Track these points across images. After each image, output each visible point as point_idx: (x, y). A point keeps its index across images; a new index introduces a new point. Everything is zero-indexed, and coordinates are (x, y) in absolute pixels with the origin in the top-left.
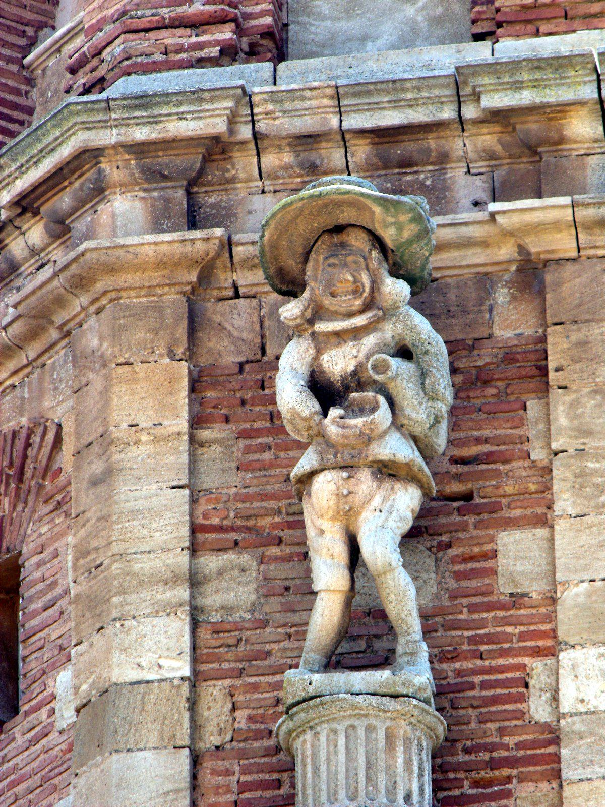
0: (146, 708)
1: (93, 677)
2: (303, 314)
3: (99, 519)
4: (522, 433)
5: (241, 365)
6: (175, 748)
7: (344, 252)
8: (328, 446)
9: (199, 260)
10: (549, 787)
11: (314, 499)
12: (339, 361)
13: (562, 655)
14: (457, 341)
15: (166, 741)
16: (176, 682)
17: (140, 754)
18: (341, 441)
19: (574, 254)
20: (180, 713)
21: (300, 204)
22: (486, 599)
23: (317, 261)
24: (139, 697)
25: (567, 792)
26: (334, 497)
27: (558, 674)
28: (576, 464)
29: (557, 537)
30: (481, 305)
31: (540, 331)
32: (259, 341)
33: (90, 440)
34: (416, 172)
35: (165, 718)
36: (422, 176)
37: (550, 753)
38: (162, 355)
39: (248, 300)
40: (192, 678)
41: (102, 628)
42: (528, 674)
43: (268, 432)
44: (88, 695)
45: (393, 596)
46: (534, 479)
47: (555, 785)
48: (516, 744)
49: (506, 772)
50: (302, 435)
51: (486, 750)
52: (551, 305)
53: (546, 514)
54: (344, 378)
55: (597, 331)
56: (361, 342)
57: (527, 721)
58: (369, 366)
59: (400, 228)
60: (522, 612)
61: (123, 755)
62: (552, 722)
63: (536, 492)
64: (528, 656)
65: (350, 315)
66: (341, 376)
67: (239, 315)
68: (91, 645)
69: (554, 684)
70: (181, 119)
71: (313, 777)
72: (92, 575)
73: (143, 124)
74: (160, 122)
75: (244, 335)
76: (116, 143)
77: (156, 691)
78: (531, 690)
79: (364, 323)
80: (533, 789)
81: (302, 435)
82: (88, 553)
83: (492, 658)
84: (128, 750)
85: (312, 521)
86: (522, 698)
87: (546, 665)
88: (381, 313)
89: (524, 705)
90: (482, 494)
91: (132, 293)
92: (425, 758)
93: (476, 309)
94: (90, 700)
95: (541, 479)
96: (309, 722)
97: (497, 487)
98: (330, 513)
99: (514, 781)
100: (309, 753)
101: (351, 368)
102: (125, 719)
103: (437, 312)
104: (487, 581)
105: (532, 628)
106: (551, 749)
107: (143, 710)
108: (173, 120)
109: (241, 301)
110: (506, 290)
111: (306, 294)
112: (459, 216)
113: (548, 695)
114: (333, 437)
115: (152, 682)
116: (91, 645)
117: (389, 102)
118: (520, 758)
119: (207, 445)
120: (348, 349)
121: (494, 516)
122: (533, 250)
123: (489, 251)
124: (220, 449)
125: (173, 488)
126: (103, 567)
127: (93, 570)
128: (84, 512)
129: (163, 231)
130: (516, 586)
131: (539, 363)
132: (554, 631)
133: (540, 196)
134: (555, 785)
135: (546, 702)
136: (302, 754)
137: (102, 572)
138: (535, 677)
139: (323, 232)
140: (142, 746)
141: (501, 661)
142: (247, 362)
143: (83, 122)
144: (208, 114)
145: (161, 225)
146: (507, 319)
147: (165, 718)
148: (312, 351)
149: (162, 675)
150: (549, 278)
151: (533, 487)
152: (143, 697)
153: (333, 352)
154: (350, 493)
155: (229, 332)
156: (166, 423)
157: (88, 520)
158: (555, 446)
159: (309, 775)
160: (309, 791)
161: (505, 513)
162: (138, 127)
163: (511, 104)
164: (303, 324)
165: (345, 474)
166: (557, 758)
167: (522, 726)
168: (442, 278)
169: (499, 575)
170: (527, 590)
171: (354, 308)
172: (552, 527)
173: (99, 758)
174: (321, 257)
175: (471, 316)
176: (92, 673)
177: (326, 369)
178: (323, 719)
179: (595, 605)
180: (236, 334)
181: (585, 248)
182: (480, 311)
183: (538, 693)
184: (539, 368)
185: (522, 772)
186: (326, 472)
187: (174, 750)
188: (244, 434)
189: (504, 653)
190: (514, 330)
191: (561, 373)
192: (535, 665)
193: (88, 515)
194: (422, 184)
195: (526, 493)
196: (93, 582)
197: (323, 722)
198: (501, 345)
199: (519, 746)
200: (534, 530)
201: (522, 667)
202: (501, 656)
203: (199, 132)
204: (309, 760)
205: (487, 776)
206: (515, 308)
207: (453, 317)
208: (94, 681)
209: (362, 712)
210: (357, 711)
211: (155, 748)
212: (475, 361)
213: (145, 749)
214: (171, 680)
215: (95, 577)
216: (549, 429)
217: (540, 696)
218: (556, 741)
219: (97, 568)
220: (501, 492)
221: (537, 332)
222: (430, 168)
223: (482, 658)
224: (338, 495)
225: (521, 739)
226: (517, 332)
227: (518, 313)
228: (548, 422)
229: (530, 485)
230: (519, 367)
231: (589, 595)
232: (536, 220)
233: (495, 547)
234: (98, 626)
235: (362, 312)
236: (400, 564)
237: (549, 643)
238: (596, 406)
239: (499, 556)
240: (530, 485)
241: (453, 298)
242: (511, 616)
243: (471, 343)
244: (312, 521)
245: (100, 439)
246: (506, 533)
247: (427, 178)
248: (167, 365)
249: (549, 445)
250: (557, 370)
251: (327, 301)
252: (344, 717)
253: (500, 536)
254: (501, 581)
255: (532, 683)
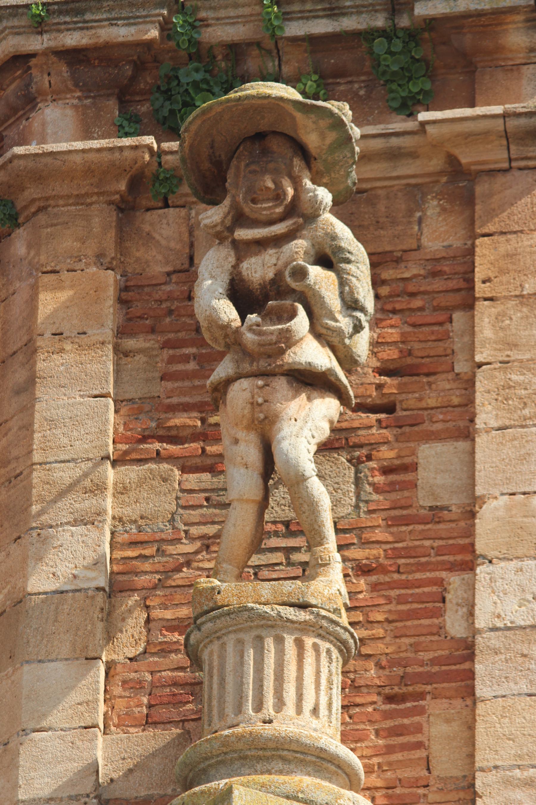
0: (59, 619)
1: (9, 586)
2: (223, 222)
3: (20, 429)
4: (446, 345)
5: (169, 274)
6: (87, 659)
7: (265, 159)
8: (244, 354)
9: (128, 169)
10: (463, 704)
11: (229, 408)
12: (259, 269)
13: (478, 570)
14: (386, 253)
15: (78, 652)
16: (90, 593)
17: (52, 665)
18: (257, 350)
19: (506, 165)
20: (93, 624)
21: (219, 109)
22: (405, 512)
23: (238, 168)
24: (53, 607)
25: (481, 708)
26: (249, 406)
27: (474, 588)
28: (500, 376)
29: (477, 450)
30: (410, 216)
31: (469, 243)
32: (187, 251)
33: (15, 348)
34: (350, 82)
35: (78, 629)
36: (356, 86)
37: (465, 670)
38: (88, 265)
39: (178, 210)
40: (107, 589)
41: (19, 538)
42: (445, 589)
43: (192, 343)
44: (3, 606)
45: (306, 506)
46: (458, 392)
47: (469, 702)
48: (430, 660)
49: (420, 688)
50: (219, 343)
51: (400, 665)
52: (480, 217)
53: (468, 427)
54: (263, 286)
55: (526, 243)
56: (281, 250)
57: (443, 636)
58: (287, 273)
59: (322, 136)
60: (441, 526)
61: (34, 666)
62: (467, 638)
63: (459, 406)
64: (445, 570)
65: (271, 222)
66: (260, 284)
67: (168, 224)
68: (8, 555)
69: (471, 598)
70: (112, 25)
71: (219, 689)
72: (12, 484)
73: (75, 29)
74: (92, 28)
75: (172, 245)
76: (47, 49)
77: (70, 601)
78: (448, 604)
79: (283, 231)
80: (446, 706)
81: (219, 343)
82: (9, 462)
83: (409, 573)
84: (40, 661)
85: (227, 429)
86: (439, 613)
87: (463, 579)
88: (301, 220)
89: (441, 620)
90: (405, 406)
91: (61, 202)
92: (334, 670)
93: (404, 220)
94: (5, 611)
95: (464, 392)
96: (216, 632)
97: (420, 399)
98: (245, 422)
99: (428, 697)
100: (215, 663)
101: (270, 275)
102: (37, 629)
103: (366, 223)
104: (406, 494)
105: (451, 542)
106: (466, 666)
107: (56, 621)
108: (104, 27)
109: (171, 210)
110: (435, 203)
111: (227, 202)
112: (391, 126)
113: (465, 610)
114: (250, 346)
115: (67, 592)
116: (8, 555)
117: (324, 10)
118: (435, 674)
119: (131, 354)
120: (267, 257)
121: (416, 428)
122: (464, 160)
123: (418, 162)
124: (144, 359)
125: (96, 397)
126: (22, 476)
127: (13, 479)
128: (6, 421)
129: (93, 138)
130: (435, 499)
131: (467, 276)
132: (473, 545)
133: (472, 105)
134: (469, 702)
135: (462, 617)
136: (209, 665)
137: (21, 481)
138: (452, 592)
139: (245, 140)
140: (53, 656)
141: (418, 576)
142: (175, 272)
143: (13, 27)
144: (140, 20)
145: (91, 132)
146: (435, 231)
147: (78, 629)
148: (232, 260)
149: (77, 585)
150: (479, 189)
151: (456, 401)
152: (57, 608)
153: (253, 260)
154: (266, 401)
155: (158, 242)
156: (90, 332)
157: (10, 430)
158: (478, 358)
159: (215, 686)
160: (215, 703)
161: (427, 426)
162: (69, 33)
163: (444, 11)
164: (223, 232)
165: (260, 383)
166: (471, 675)
167: (437, 641)
168: (372, 189)
169: (419, 487)
170: (445, 503)
171: (274, 216)
172: (473, 440)
173: (10, 669)
174: (243, 164)
175: (400, 228)
176: (7, 583)
177: (246, 277)
178: (230, 629)
179: (515, 520)
180: (163, 242)
181: (516, 159)
182: (410, 223)
183: (455, 608)
184: (466, 280)
185: (436, 688)
186: (242, 380)
187: (86, 661)
188: (167, 345)
189: (422, 567)
190: (443, 242)
191: (488, 284)
192: (452, 579)
193: (10, 424)
194: (356, 94)
195: (449, 406)
196: (13, 491)
197: (230, 632)
198: (428, 257)
199: (434, 662)
200: (455, 443)
201: (440, 582)
202: (418, 571)
203: (130, 39)
204: (215, 671)
205: (401, 691)
206: (444, 220)
207: (382, 228)
208: (9, 591)
209: (270, 623)
210: (263, 622)
211: (66, 659)
212: (402, 273)
213: (56, 660)
214: (86, 590)
215: (14, 486)
216: (473, 342)
217: (457, 611)
218: (471, 657)
219: (16, 477)
220: (423, 404)
221: (466, 244)
222: (363, 78)
223: (399, 572)
224: (252, 404)
225: (436, 655)
226: (445, 244)
227: (447, 224)
228: (473, 334)
229: (454, 397)
230: (446, 279)
231: (509, 508)
232: (467, 130)
233: (415, 460)
234: (15, 535)
235: (282, 219)
236: (315, 474)
237: (468, 557)
238: (522, 318)
239: (419, 469)
240: (454, 397)
241: (383, 209)
242: (429, 530)
243: (399, 254)
244: (227, 429)
245: (24, 348)
246: (427, 445)
247: (361, 88)
248: (94, 274)
249: (473, 357)
250: (484, 282)
251: (248, 209)
252: (251, 627)
253: (421, 448)
254: (421, 493)
255: (448, 597)
